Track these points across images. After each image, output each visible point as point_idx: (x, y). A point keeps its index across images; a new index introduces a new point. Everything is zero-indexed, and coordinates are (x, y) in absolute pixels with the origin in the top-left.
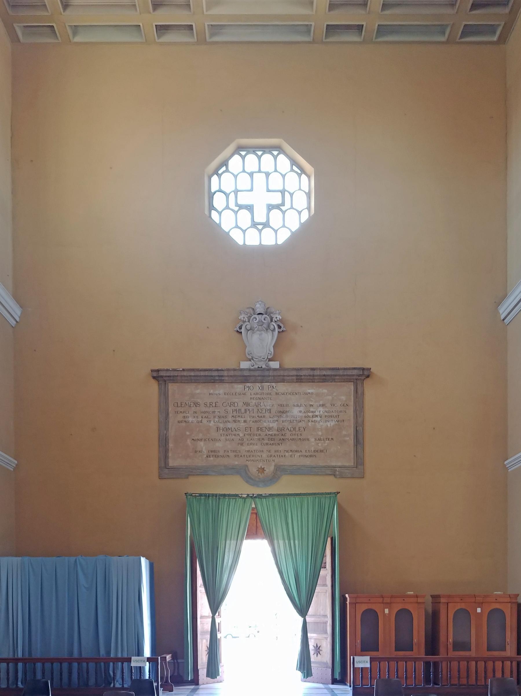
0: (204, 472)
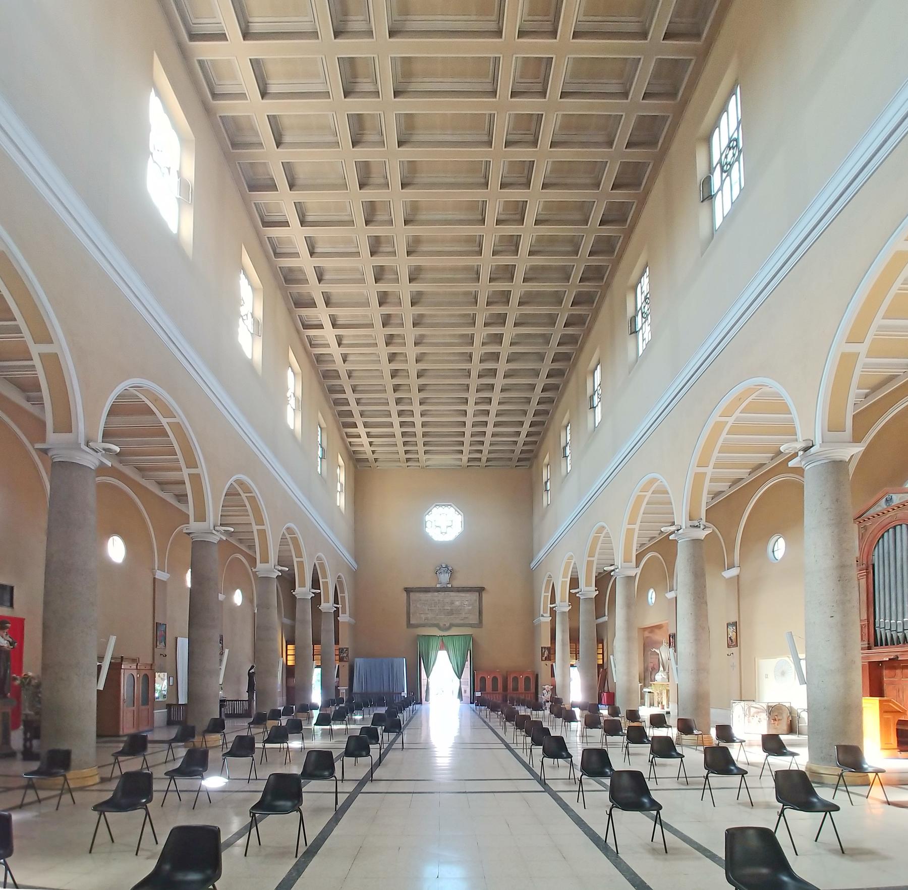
0: (424, 626)
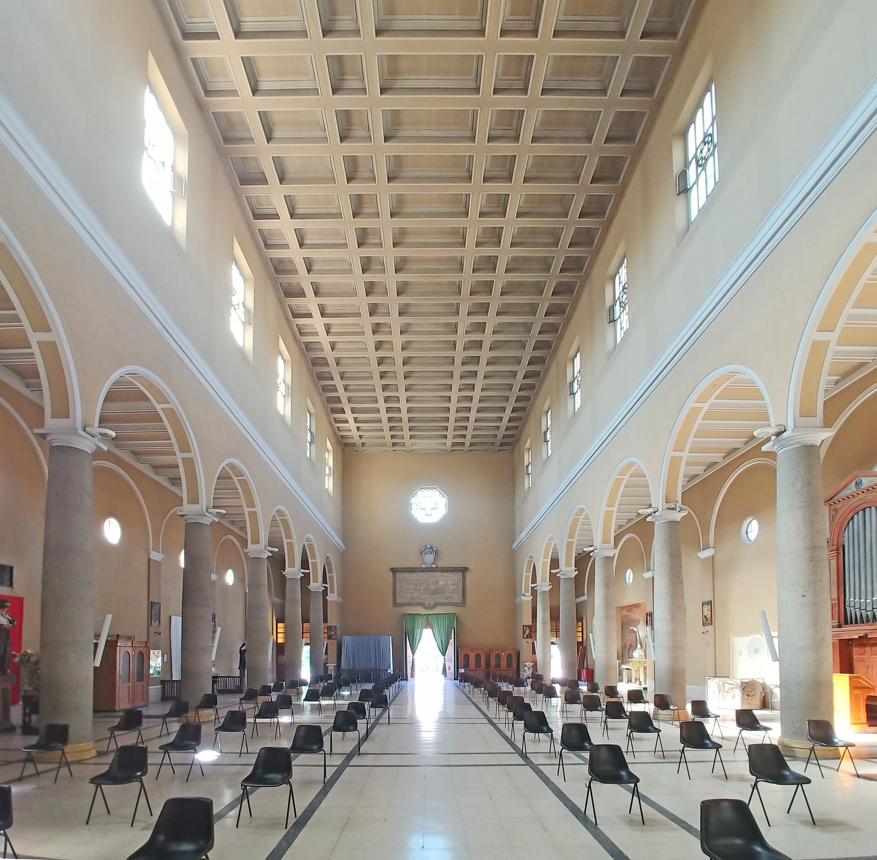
0: (409, 605)
